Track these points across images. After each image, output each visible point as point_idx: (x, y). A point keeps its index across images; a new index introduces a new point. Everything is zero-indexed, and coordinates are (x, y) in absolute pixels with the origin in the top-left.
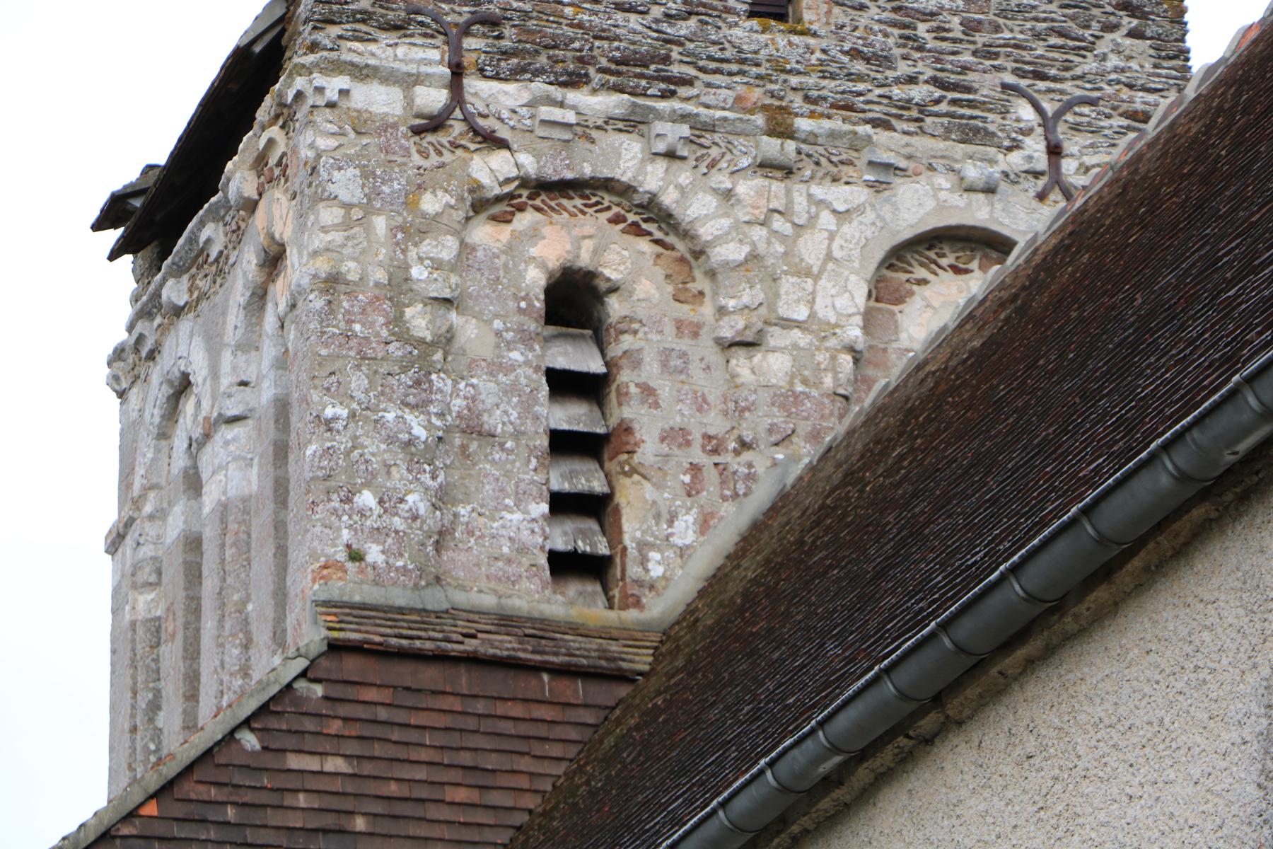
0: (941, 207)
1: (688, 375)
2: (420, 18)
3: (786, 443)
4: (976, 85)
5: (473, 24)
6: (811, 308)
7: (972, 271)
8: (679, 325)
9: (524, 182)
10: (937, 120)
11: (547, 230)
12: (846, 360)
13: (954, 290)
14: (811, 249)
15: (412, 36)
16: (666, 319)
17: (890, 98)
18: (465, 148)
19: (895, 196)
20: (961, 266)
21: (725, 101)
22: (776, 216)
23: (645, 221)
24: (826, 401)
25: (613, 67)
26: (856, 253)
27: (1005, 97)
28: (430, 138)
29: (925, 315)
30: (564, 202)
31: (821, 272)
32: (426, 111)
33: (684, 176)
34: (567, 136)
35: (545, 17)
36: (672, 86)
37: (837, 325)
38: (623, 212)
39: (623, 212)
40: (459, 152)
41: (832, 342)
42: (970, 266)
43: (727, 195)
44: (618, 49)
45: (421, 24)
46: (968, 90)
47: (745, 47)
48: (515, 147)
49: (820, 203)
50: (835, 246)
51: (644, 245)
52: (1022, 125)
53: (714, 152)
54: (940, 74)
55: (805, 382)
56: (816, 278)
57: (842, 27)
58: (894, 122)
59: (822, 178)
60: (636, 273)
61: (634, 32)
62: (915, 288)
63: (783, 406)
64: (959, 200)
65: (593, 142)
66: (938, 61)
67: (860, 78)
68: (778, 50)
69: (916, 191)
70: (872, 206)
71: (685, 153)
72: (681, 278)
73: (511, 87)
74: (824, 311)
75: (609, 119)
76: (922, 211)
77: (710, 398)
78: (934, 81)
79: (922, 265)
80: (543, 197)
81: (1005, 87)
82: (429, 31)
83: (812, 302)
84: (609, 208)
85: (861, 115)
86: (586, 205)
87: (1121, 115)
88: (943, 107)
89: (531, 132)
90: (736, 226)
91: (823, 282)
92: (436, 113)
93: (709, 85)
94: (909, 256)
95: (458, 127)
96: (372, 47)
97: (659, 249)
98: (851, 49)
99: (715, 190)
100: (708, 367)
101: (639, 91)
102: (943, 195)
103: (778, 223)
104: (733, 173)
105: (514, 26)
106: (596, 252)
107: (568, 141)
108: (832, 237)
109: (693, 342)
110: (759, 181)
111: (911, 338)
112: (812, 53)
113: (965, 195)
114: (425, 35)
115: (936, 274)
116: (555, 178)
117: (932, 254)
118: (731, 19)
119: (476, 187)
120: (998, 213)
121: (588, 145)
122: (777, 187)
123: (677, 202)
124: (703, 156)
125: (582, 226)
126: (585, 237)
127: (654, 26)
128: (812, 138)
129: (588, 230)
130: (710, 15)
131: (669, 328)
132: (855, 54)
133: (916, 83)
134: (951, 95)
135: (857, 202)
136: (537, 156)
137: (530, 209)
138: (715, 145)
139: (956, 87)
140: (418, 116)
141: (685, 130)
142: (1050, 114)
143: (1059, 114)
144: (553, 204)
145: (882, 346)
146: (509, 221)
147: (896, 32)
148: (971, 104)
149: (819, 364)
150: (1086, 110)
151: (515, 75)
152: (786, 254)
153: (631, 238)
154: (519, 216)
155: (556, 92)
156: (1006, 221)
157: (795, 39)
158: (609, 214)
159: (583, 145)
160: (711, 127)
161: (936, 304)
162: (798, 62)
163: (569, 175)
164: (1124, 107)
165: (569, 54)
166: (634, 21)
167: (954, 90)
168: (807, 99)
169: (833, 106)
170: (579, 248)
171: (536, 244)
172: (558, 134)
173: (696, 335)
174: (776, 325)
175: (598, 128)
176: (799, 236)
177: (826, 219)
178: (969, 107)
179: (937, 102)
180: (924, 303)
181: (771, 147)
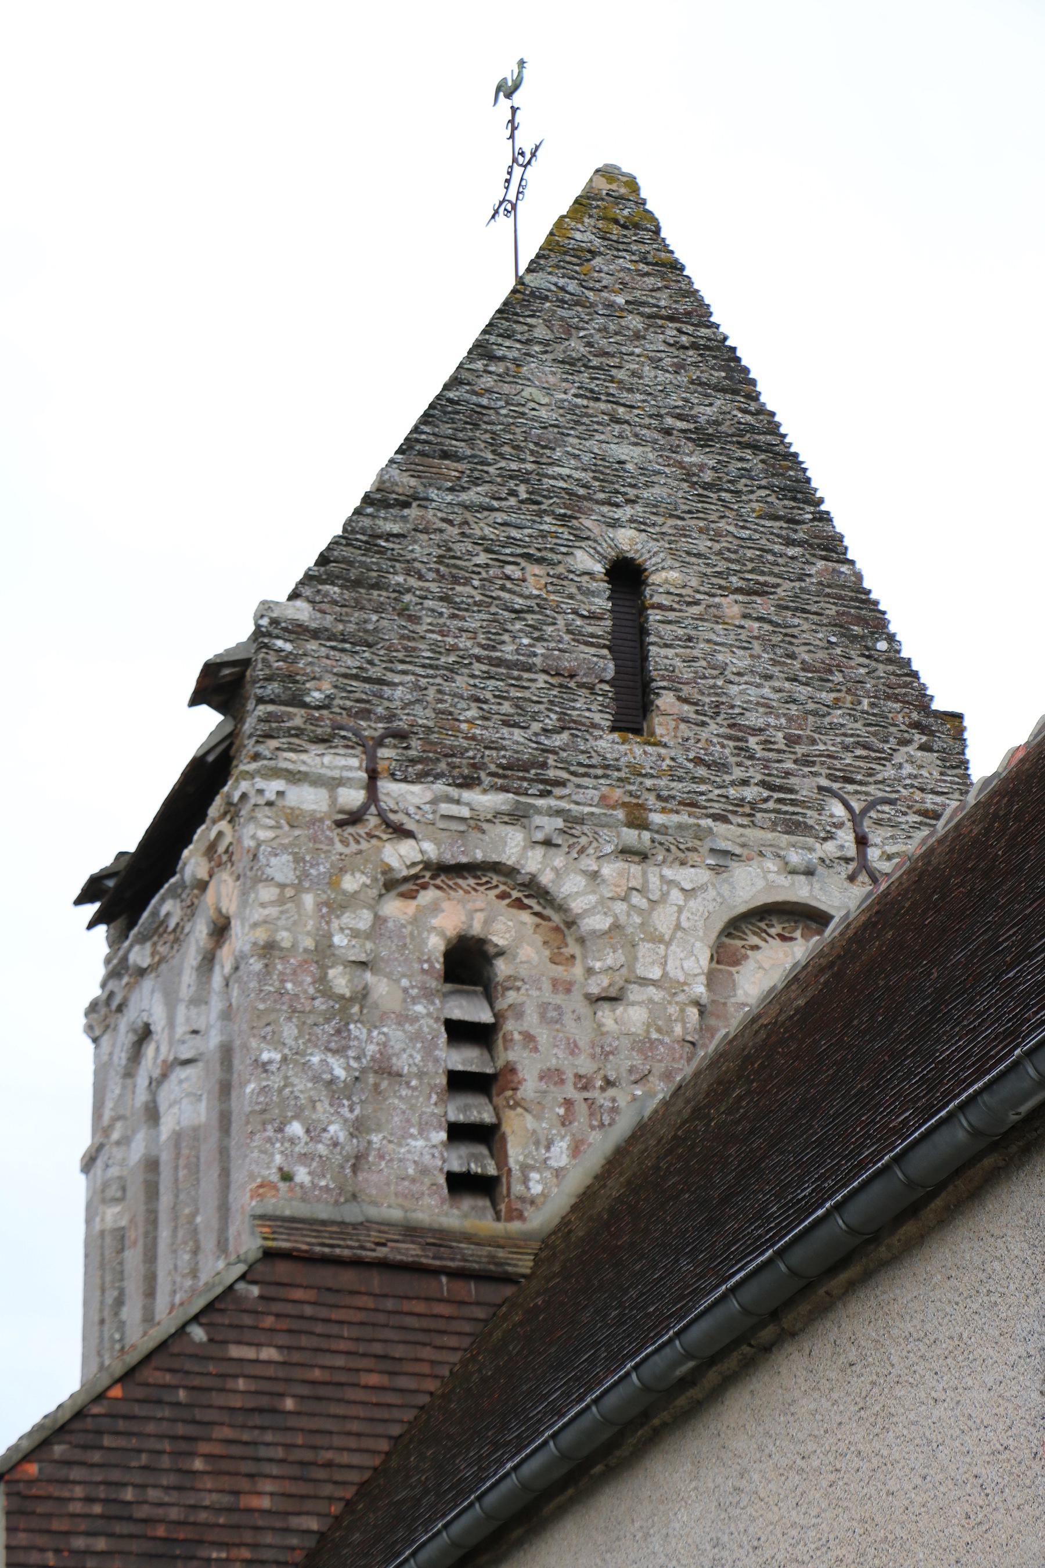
0: (770, 886)
1: (562, 1025)
2: (343, 733)
3: (644, 1081)
4: (797, 788)
5: (387, 737)
6: (664, 969)
7: (796, 939)
8: (555, 983)
9: (427, 865)
10: (766, 815)
11: (445, 905)
12: (693, 1012)
13: (781, 955)
14: (663, 920)
15: (336, 747)
16: (544, 978)
17: (727, 797)
18: (379, 838)
19: (732, 877)
20: (787, 935)
21: (592, 799)
22: (634, 892)
23: (527, 897)
24: (676, 1046)
25: (501, 771)
26: (700, 924)
27: (821, 797)
28: (350, 830)
29: (757, 976)
30: (460, 881)
31: (671, 940)
32: (347, 808)
33: (559, 860)
34: (462, 828)
35: (445, 732)
36: (549, 787)
37: (685, 983)
38: (508, 890)
39: (508, 890)
40: (374, 841)
41: (681, 998)
42: (794, 935)
43: (594, 876)
44: (504, 757)
45: (344, 737)
46: (791, 791)
47: (608, 756)
48: (420, 836)
49: (671, 883)
50: (683, 917)
51: (526, 917)
52: (835, 820)
53: (584, 840)
54: (767, 778)
55: (659, 1030)
56: (668, 944)
57: (687, 740)
58: (730, 816)
59: (672, 862)
60: (519, 939)
61: (518, 743)
62: (749, 953)
63: (641, 1051)
64: (784, 880)
65: (483, 832)
66: (766, 767)
67: (702, 781)
68: (635, 758)
69: (750, 873)
70: (713, 885)
71: (560, 842)
72: (556, 944)
73: (416, 788)
74: (674, 971)
75: (497, 814)
76: (754, 890)
77: (581, 1044)
78: (763, 784)
79: (755, 933)
80: (443, 877)
81: (820, 788)
82: (350, 744)
83: (664, 964)
84: (497, 886)
85: (704, 811)
86: (478, 884)
87: (915, 813)
88: (771, 805)
89: (433, 824)
90: (602, 901)
91: (673, 948)
92: (355, 809)
93: (579, 786)
94: (744, 927)
95: (373, 821)
96: (304, 757)
97: (538, 920)
98: (695, 757)
99: (583, 871)
100: (579, 1018)
101: (521, 791)
102: (771, 877)
103: (636, 899)
104: (599, 858)
105: (420, 739)
106: (487, 922)
107: (463, 832)
108: (680, 910)
109: (566, 997)
110: (620, 865)
111: (746, 994)
112: (663, 760)
113: (789, 877)
114: (347, 747)
115: (766, 941)
116: (453, 862)
117: (763, 925)
118: (597, 733)
119: (388, 870)
120: (817, 892)
121: (480, 835)
122: (635, 869)
123: (553, 882)
124: (574, 843)
125: (474, 901)
126: (477, 911)
127: (534, 738)
128: (663, 830)
129: (480, 904)
130: (579, 730)
131: (547, 986)
132: (698, 761)
133: (748, 785)
134: (776, 795)
135: (701, 882)
136: (438, 843)
137: (432, 888)
138: (584, 835)
139: (780, 789)
140: (341, 812)
141: (559, 823)
142: (857, 812)
143: (864, 812)
144: (451, 883)
145: (723, 1001)
146: (414, 898)
147: (731, 744)
148: (793, 803)
149: (670, 1015)
150: (886, 808)
151: (420, 778)
152: (642, 924)
153: (514, 911)
154: (422, 893)
155: (454, 792)
156: (823, 898)
157: (649, 749)
158: (497, 891)
159: (475, 835)
160: (580, 820)
161: (766, 966)
162: (651, 768)
163: (464, 860)
164: (918, 806)
165: (464, 761)
166: (518, 734)
167: (779, 791)
168: (659, 797)
169: (680, 803)
170: (472, 919)
171: (436, 916)
172: (455, 826)
173: (568, 991)
174: (635, 983)
175: (488, 821)
176: (652, 909)
177: (675, 895)
178: (792, 805)
179: (766, 800)
180: (757, 965)
181: (631, 836)
